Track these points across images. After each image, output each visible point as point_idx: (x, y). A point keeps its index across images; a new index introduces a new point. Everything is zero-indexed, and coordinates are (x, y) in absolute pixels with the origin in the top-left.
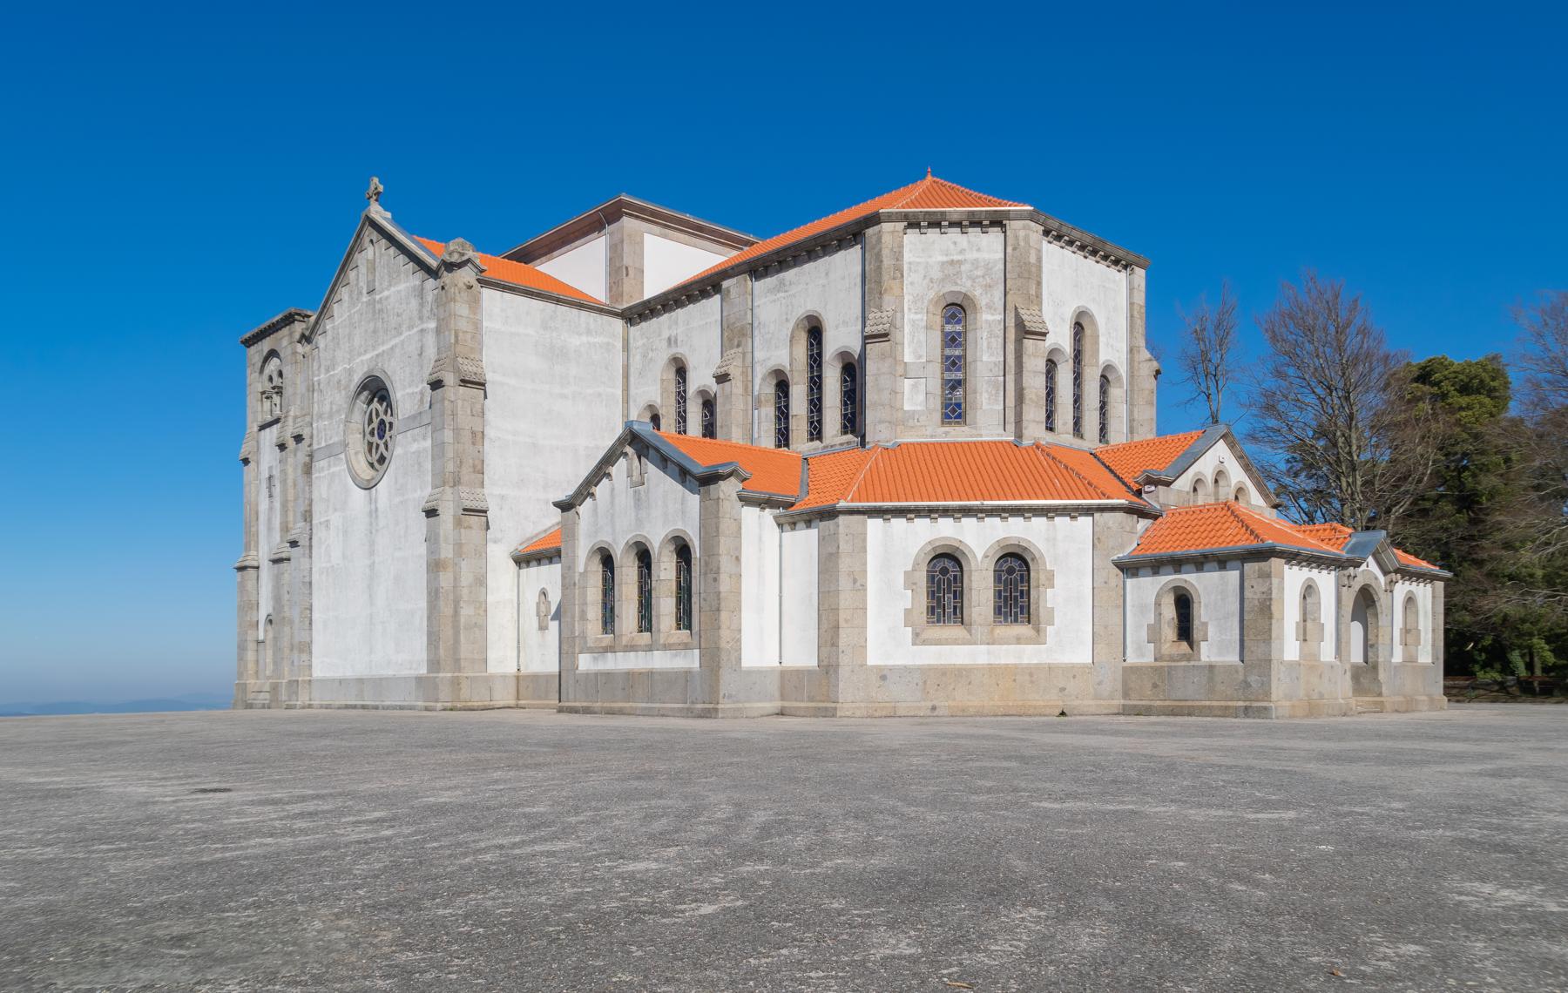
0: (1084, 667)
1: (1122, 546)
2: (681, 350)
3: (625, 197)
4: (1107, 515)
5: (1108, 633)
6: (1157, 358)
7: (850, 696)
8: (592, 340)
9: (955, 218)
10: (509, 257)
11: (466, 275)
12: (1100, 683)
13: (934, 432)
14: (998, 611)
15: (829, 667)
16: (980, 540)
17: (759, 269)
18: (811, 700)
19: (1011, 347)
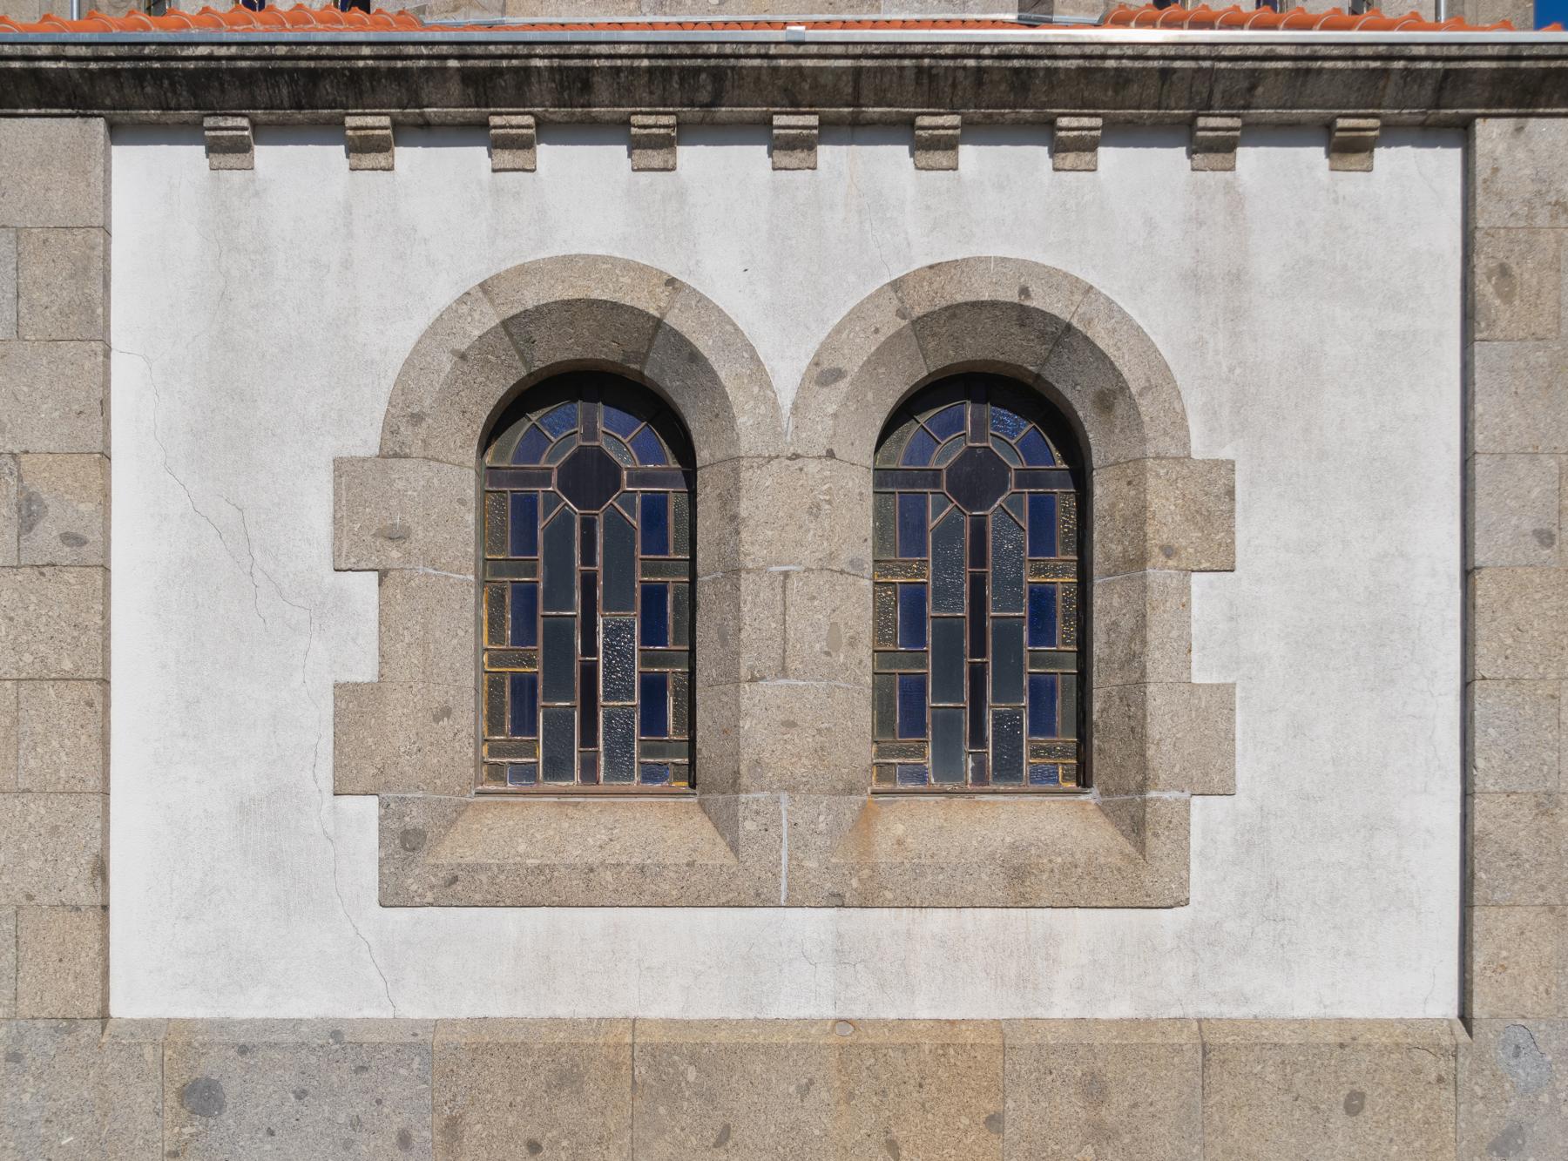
0: (1404, 1044)
14: (902, 710)
16: (784, 270)
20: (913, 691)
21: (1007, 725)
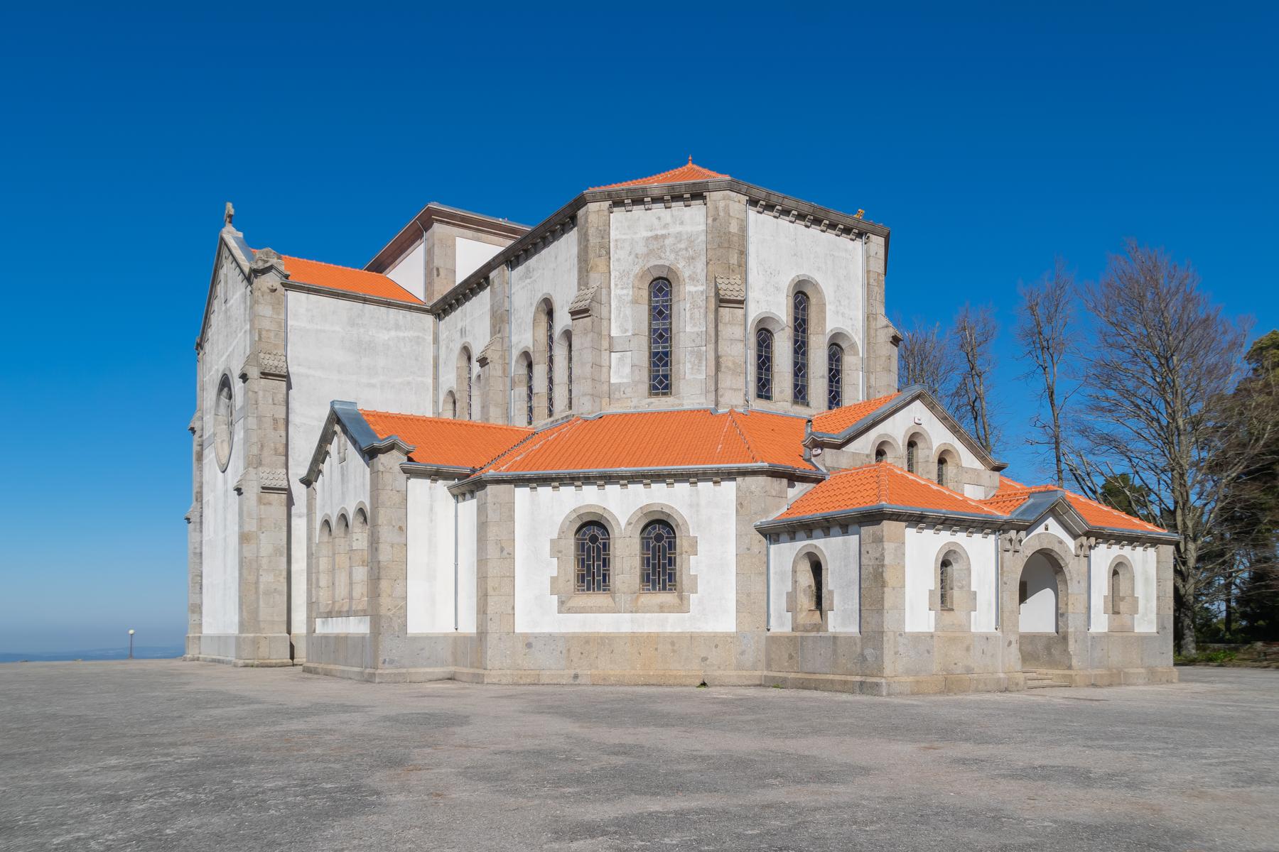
1: (766, 511)
2: (469, 339)
3: (434, 205)
4: (749, 479)
5: (752, 602)
6: (897, 324)
7: (498, 663)
8: (401, 334)
9: (656, 193)
11: (271, 280)
12: (742, 653)
13: (638, 400)
15: (482, 634)
16: (623, 506)
17: (512, 259)
18: (472, 666)
19: (712, 316)
20: (648, 575)
21: (664, 581)
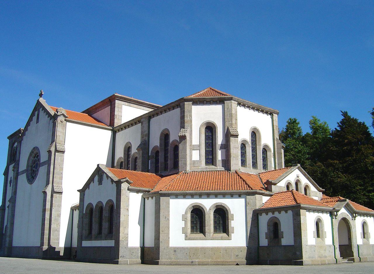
10: (83, 112)
